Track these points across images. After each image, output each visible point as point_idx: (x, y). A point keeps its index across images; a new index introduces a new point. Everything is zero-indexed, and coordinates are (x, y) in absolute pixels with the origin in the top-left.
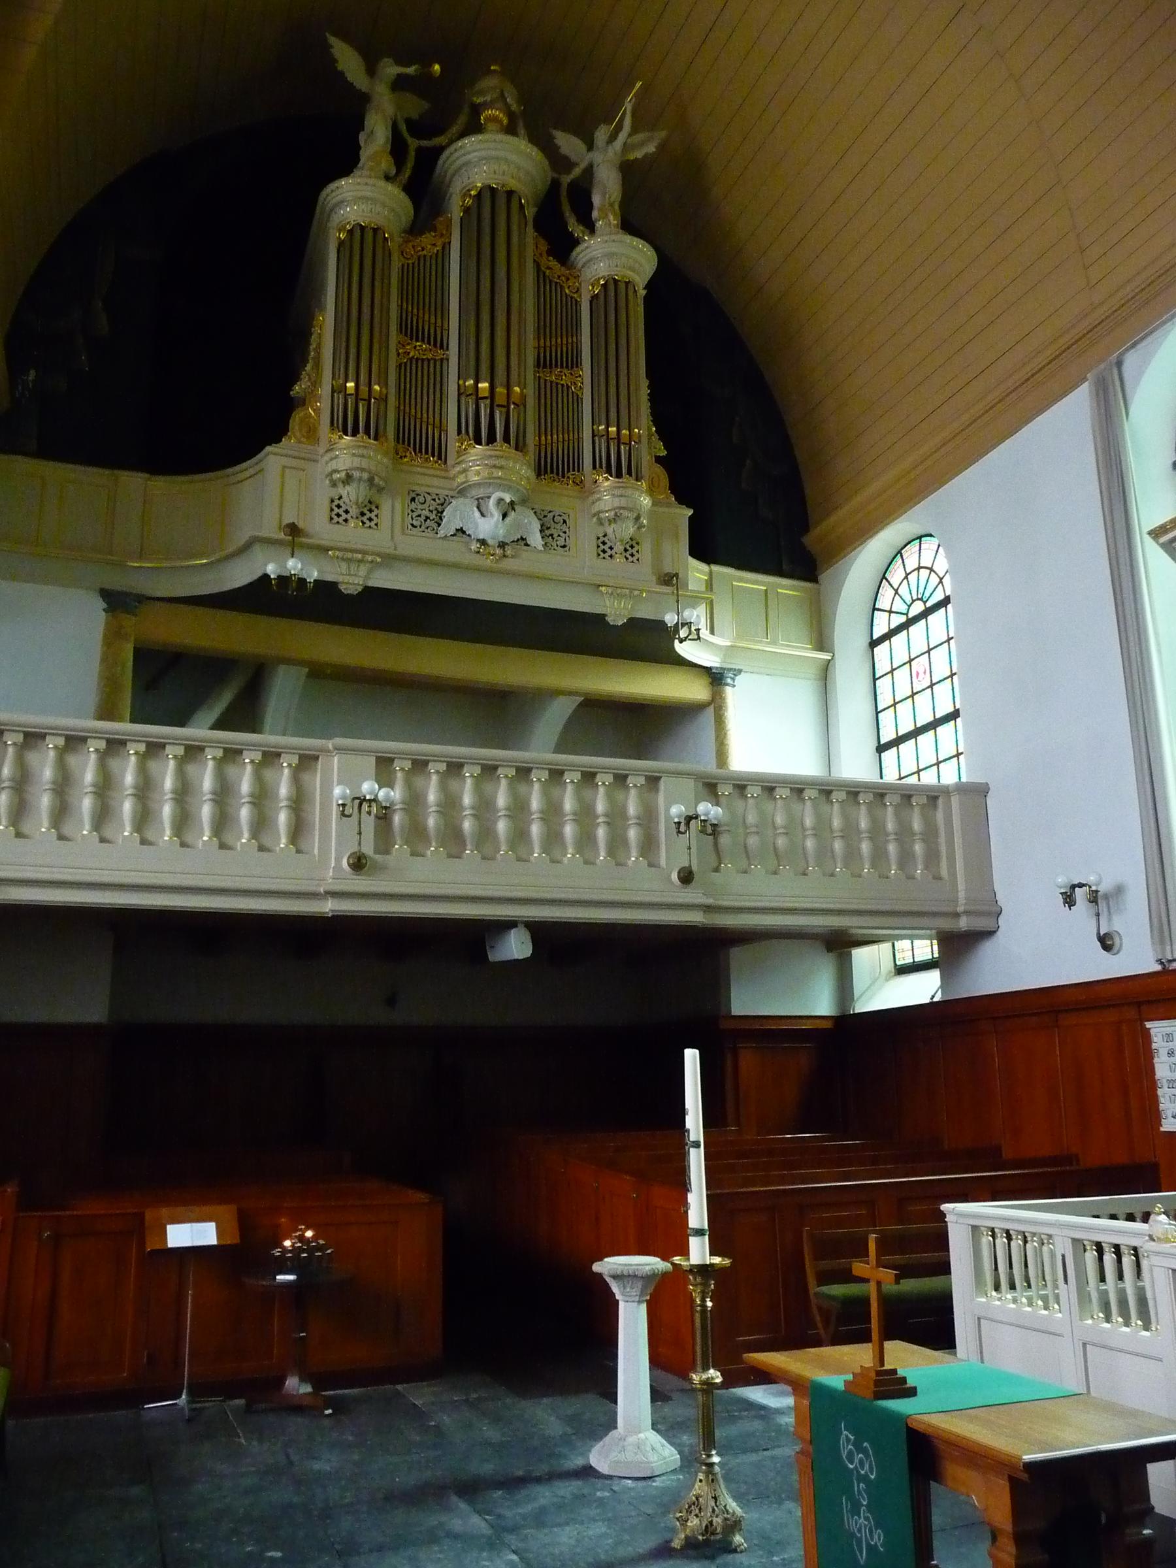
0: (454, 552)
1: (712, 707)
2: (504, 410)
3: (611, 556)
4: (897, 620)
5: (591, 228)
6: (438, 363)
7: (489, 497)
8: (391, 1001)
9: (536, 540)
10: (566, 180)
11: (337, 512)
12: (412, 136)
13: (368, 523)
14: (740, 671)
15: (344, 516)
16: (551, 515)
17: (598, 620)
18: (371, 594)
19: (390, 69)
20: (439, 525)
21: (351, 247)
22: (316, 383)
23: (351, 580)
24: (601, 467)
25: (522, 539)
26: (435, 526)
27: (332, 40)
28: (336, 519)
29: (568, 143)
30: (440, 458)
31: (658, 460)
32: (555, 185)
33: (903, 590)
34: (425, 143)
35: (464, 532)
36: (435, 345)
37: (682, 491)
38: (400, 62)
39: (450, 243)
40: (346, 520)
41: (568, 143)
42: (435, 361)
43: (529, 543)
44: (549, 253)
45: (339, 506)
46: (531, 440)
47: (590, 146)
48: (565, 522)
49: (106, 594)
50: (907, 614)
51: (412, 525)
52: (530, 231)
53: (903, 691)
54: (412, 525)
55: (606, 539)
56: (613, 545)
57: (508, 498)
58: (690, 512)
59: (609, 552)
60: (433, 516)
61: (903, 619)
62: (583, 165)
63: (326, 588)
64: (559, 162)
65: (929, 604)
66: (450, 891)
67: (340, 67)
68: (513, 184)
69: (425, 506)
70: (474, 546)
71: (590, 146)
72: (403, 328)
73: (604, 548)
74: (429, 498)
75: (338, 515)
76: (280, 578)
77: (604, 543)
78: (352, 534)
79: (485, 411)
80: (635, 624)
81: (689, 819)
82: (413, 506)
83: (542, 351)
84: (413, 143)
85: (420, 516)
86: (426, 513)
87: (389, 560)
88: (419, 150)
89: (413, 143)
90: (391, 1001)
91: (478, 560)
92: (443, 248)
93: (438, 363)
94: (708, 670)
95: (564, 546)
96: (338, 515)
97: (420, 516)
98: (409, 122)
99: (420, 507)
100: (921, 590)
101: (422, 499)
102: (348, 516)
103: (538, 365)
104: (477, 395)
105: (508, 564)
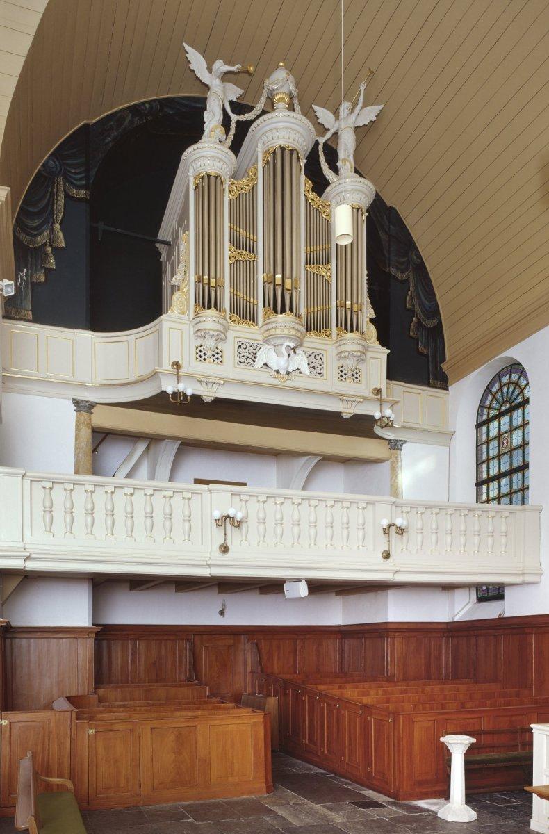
0: (265, 377)
1: (389, 462)
2: (290, 292)
3: (345, 379)
4: (492, 413)
5: (336, 170)
6: (252, 263)
7: (282, 345)
8: (222, 613)
9: (306, 370)
10: (322, 140)
11: (201, 355)
12: (233, 112)
13: (216, 361)
14: (405, 442)
15: (204, 356)
16: (313, 355)
17: (338, 415)
18: (218, 401)
19: (221, 67)
20: (254, 362)
21: (203, 187)
22: (185, 278)
23: (208, 394)
24: (341, 326)
25: (298, 369)
26: (252, 362)
27: (187, 48)
28: (199, 359)
29: (324, 115)
30: (254, 322)
31: (372, 321)
32: (317, 143)
33: (499, 395)
34: (243, 118)
35: (267, 366)
36: (250, 251)
37: (383, 340)
38: (227, 63)
39: (256, 184)
40: (205, 359)
41: (324, 115)
42: (250, 262)
43: (258, 355)
44: (313, 190)
45: (200, 351)
46: (303, 310)
47: (336, 113)
48: (321, 358)
49: (76, 402)
50: (499, 410)
51: (240, 362)
52: (303, 177)
53: (493, 453)
54: (240, 362)
55: (202, 349)
56: (346, 372)
57: (292, 345)
58: (389, 351)
59: (344, 377)
60: (250, 356)
61: (496, 412)
62: (332, 131)
63: (196, 398)
64: (322, 129)
65: (513, 404)
66: (281, 564)
67: (389, 204)
68: (294, 145)
69: (246, 350)
70: (274, 374)
71: (336, 113)
72: (233, 241)
73: (342, 375)
74: (248, 345)
75: (201, 356)
76: (174, 394)
77: (342, 371)
78: (209, 368)
79: (187, 248)
80: (357, 418)
81: (390, 526)
82: (240, 350)
83: (308, 254)
84: (234, 118)
85: (243, 356)
86: (248, 354)
87: (228, 382)
88: (238, 123)
89: (234, 118)
90: (222, 613)
91: (275, 382)
92: (253, 188)
93: (252, 263)
94: (389, 441)
95: (320, 373)
96: (201, 356)
97: (243, 356)
98: (231, 102)
99: (245, 351)
100: (510, 395)
101: (244, 346)
102: (206, 357)
103: (307, 264)
104: (275, 282)
105: (289, 383)
